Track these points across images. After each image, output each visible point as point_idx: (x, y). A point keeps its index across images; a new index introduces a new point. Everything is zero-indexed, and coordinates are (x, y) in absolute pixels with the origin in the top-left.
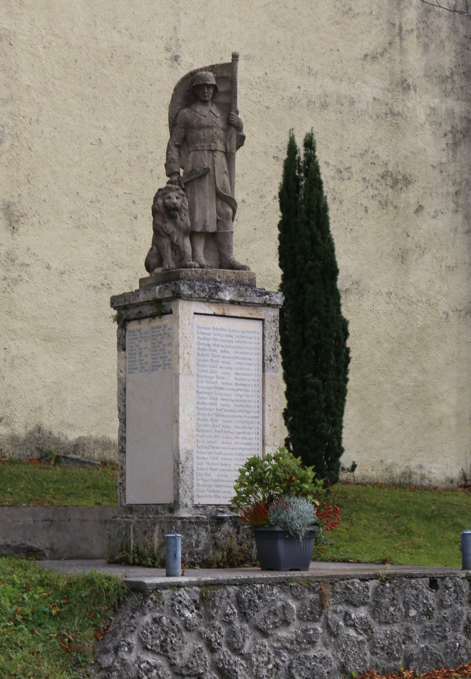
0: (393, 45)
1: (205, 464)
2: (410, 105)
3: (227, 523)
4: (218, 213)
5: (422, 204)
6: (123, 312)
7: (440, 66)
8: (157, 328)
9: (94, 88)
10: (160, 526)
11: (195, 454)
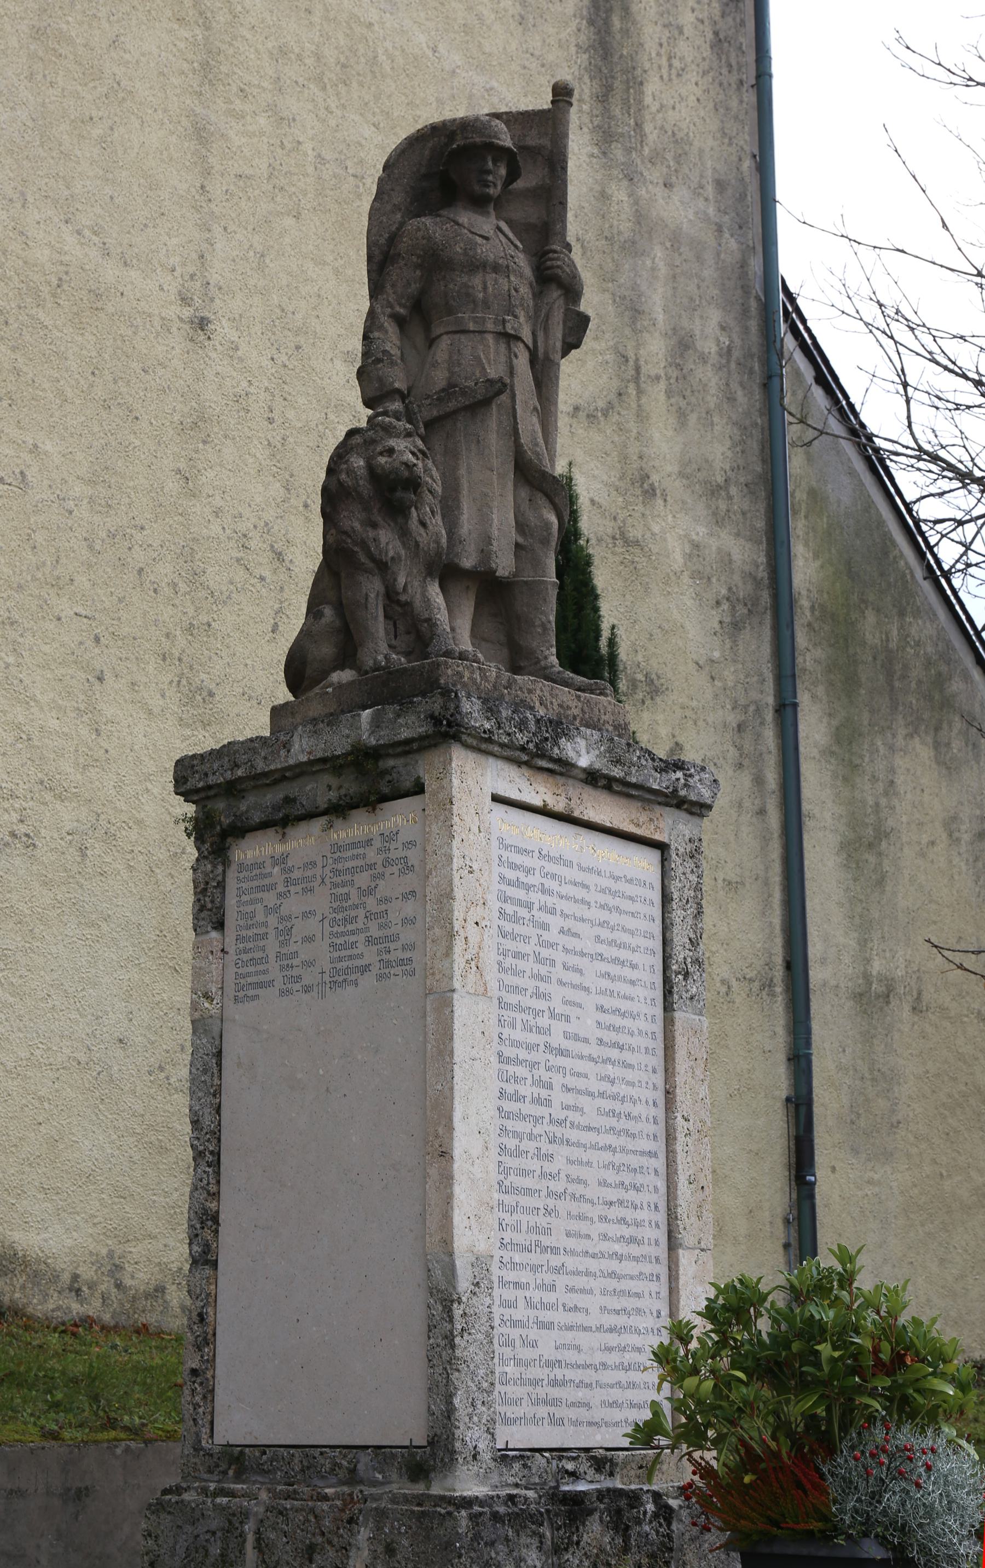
0: (624, 397)
1: (521, 1303)
2: (656, 529)
3: (597, 1516)
4: (521, 527)
5: (681, 739)
6: (220, 805)
7: (707, 461)
8: (354, 845)
9: (14, 349)
10: (379, 1529)
11: (496, 1272)
